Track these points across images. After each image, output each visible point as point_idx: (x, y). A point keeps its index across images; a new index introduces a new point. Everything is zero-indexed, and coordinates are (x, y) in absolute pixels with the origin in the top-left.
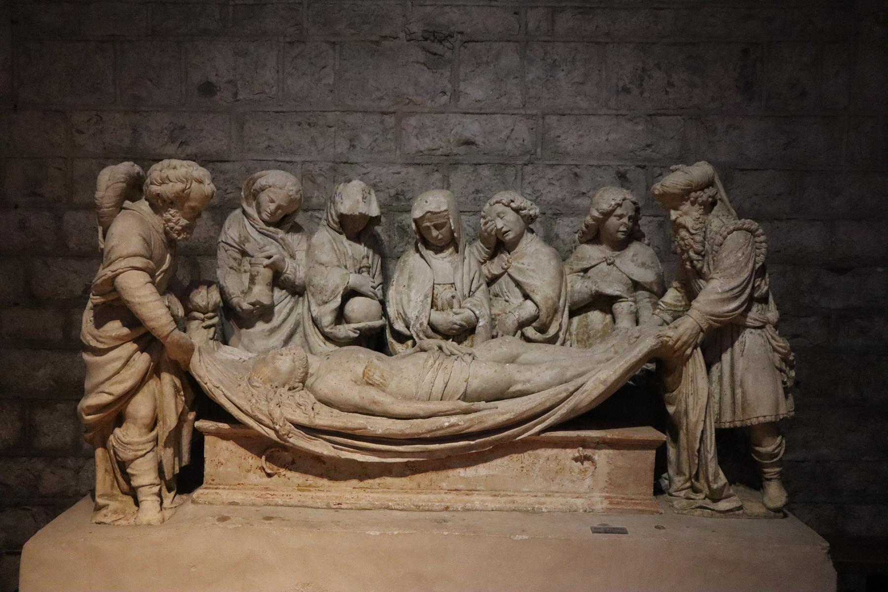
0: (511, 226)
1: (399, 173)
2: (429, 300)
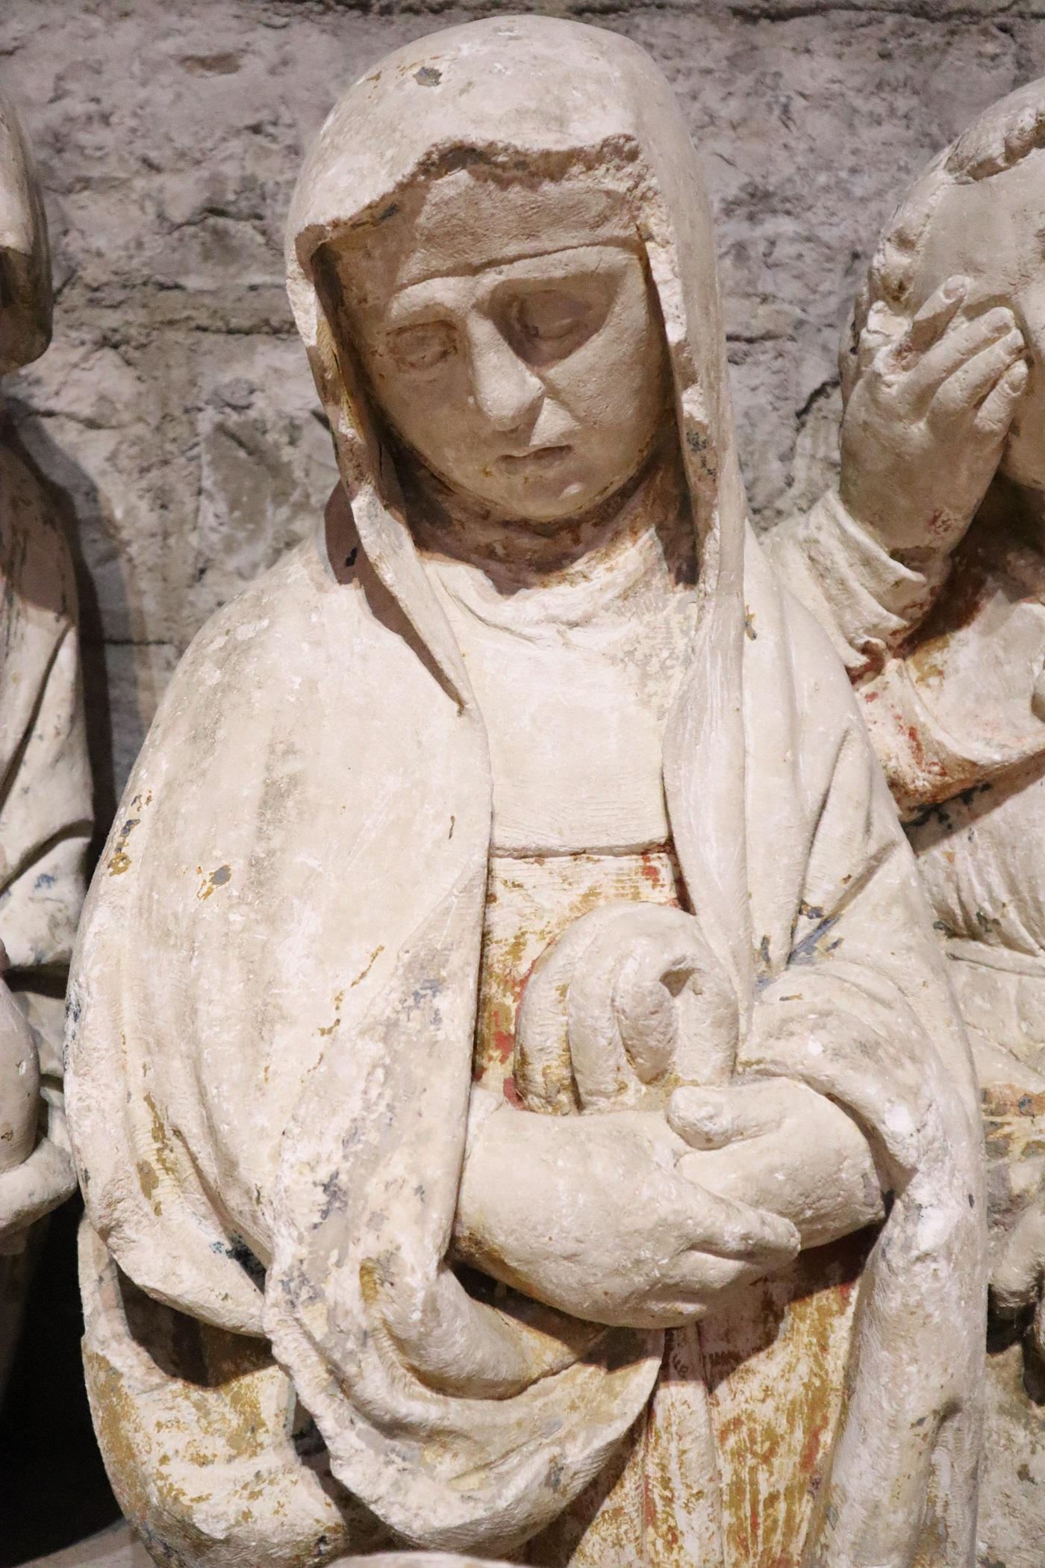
1: (224, 63)
2: (455, 1009)
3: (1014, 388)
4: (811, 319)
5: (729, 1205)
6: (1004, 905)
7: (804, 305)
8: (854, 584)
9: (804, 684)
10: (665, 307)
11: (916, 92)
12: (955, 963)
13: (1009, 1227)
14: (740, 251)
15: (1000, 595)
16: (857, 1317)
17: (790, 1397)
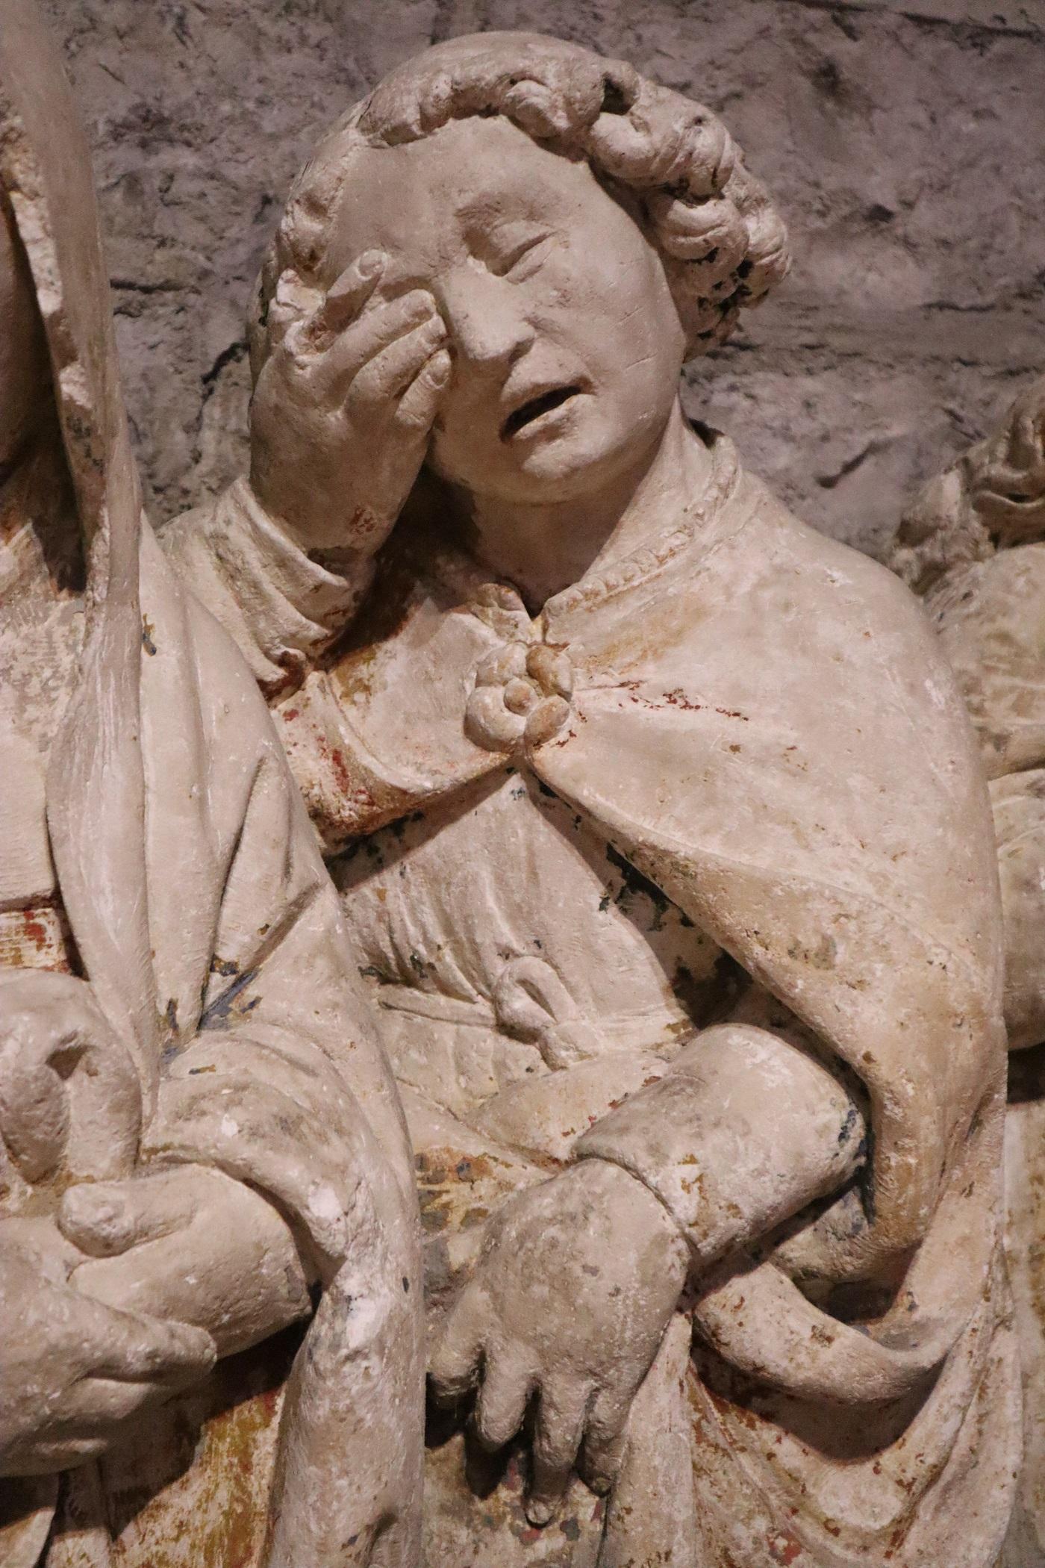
0: (599, 336)
3: (438, 380)
4: (217, 269)
5: (133, 1319)
6: (439, 948)
7: (209, 253)
8: (269, 588)
9: (213, 706)
10: (35, 270)
11: (328, 19)
12: (387, 1012)
13: (448, 1307)
14: (132, 183)
15: (429, 602)
16: (283, 1428)
17: (208, 1530)
